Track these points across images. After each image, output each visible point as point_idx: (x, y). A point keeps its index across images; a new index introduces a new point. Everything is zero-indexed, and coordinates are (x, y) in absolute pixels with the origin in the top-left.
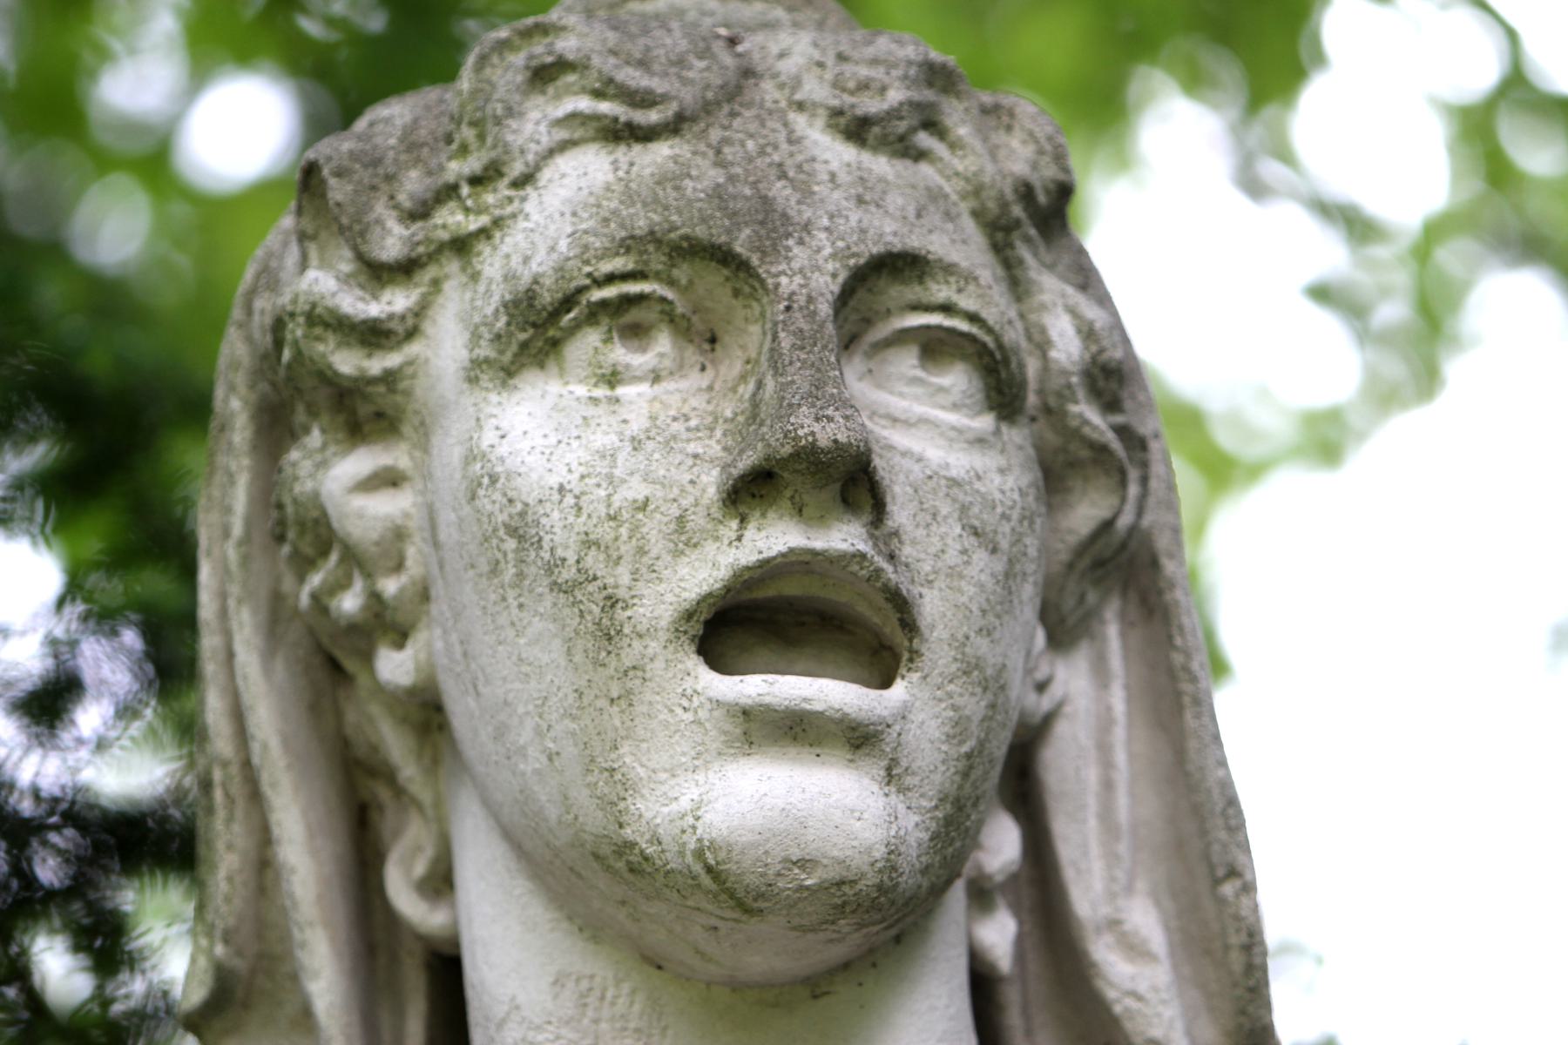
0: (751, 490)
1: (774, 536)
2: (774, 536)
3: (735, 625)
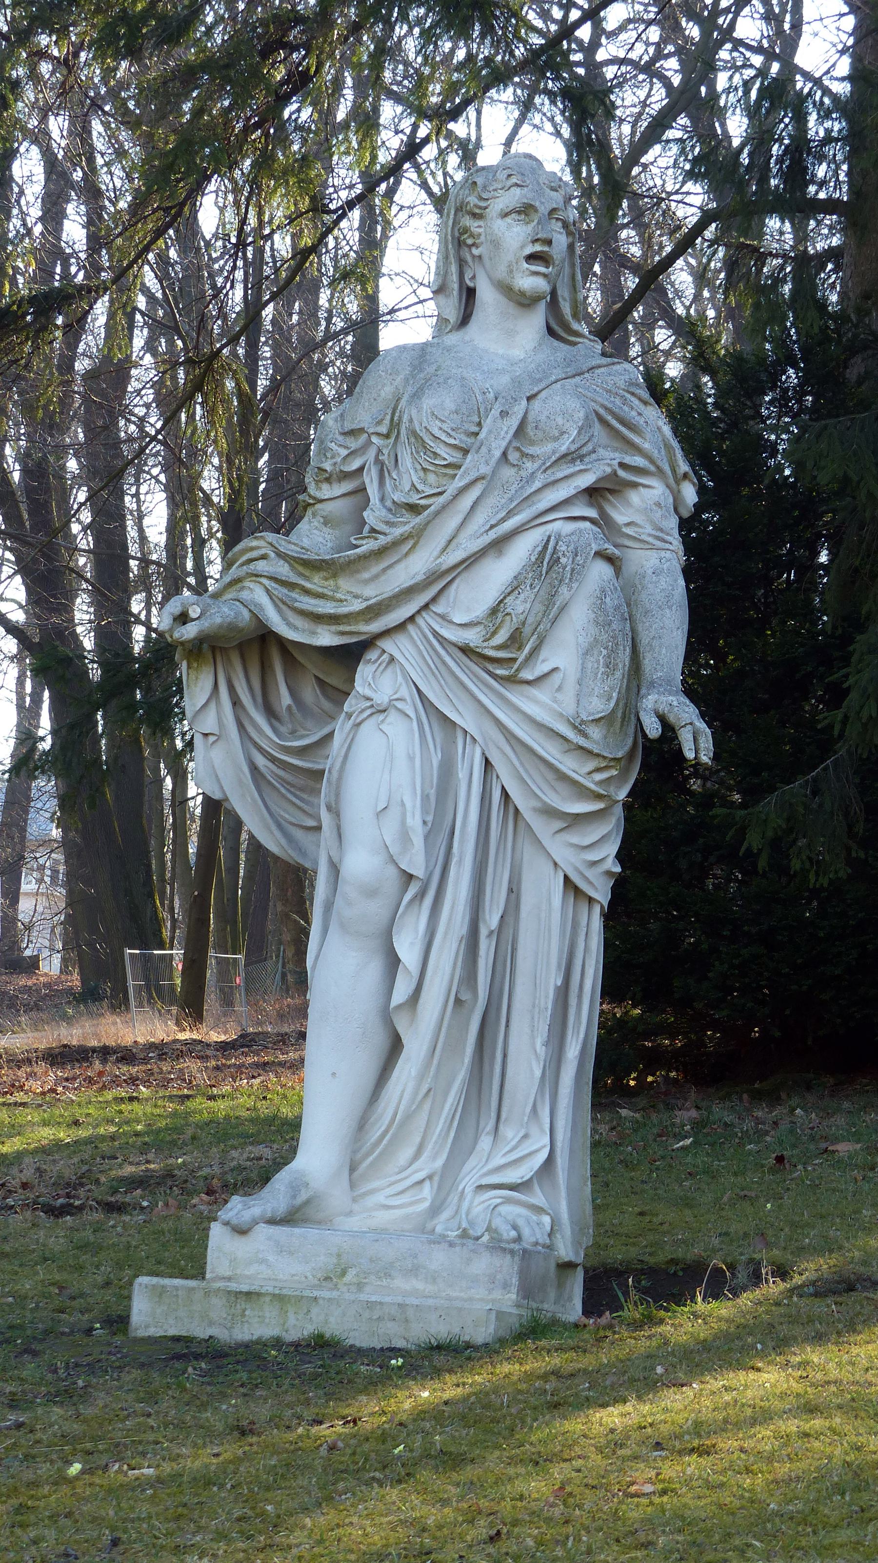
1: (538, 248)
3: (532, 258)
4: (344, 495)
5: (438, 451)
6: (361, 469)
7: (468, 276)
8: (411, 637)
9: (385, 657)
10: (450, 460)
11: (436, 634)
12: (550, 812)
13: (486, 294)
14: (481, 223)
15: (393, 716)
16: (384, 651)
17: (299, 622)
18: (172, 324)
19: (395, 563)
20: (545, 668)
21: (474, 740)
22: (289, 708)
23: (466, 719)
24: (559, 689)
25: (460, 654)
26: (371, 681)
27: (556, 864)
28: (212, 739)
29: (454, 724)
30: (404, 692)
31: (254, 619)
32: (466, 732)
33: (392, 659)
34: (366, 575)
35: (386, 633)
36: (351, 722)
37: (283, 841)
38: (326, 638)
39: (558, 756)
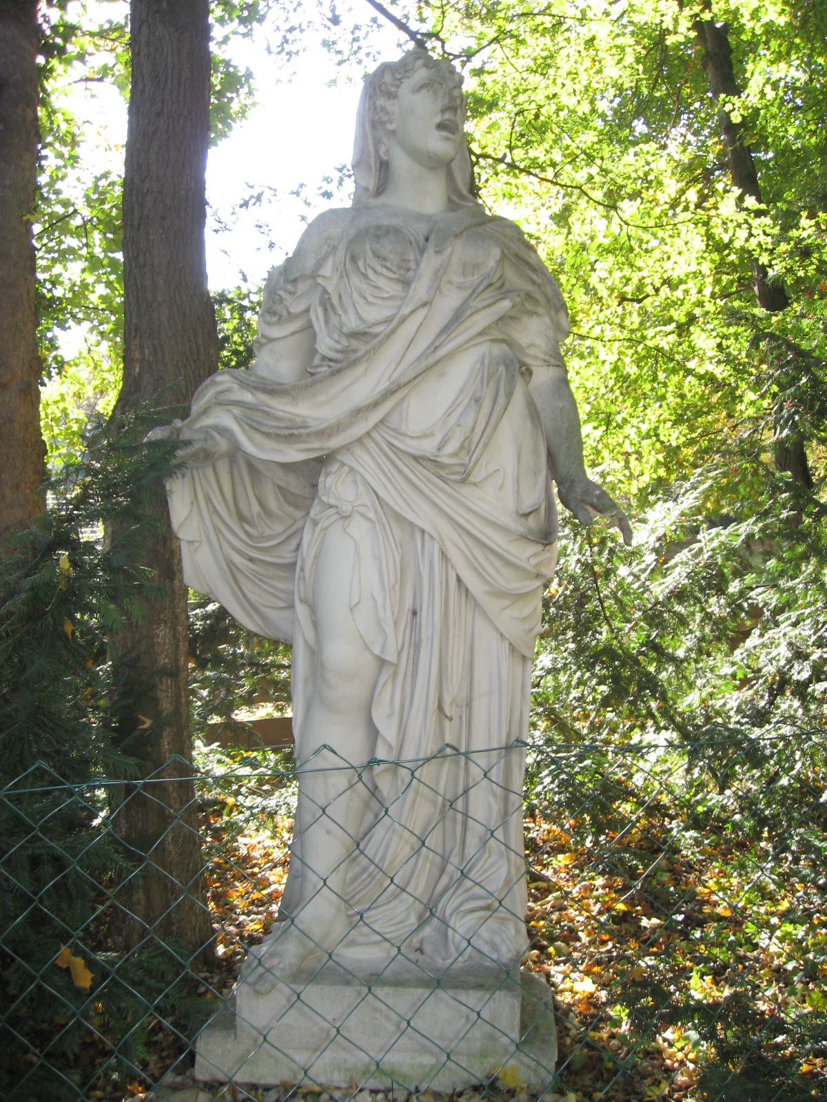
0: (443, 111)
2: (447, 116)
4: (293, 334)
5: (380, 285)
6: (307, 311)
7: (382, 150)
8: (367, 450)
9: (346, 469)
10: (392, 293)
11: (391, 445)
12: (499, 594)
13: (401, 162)
14: (395, 101)
15: (357, 517)
16: (343, 464)
17: (268, 443)
18: (305, 800)
19: (351, 385)
20: (491, 468)
21: (431, 537)
22: (259, 515)
23: (423, 516)
24: (501, 487)
25: (413, 462)
26: (337, 487)
27: (502, 635)
28: (196, 545)
29: (412, 524)
30: (366, 499)
31: (424, 91)
32: (423, 531)
33: (352, 469)
34: (322, 398)
35: (347, 447)
36: (318, 529)
37: (260, 622)
38: (294, 454)
39: (505, 546)
